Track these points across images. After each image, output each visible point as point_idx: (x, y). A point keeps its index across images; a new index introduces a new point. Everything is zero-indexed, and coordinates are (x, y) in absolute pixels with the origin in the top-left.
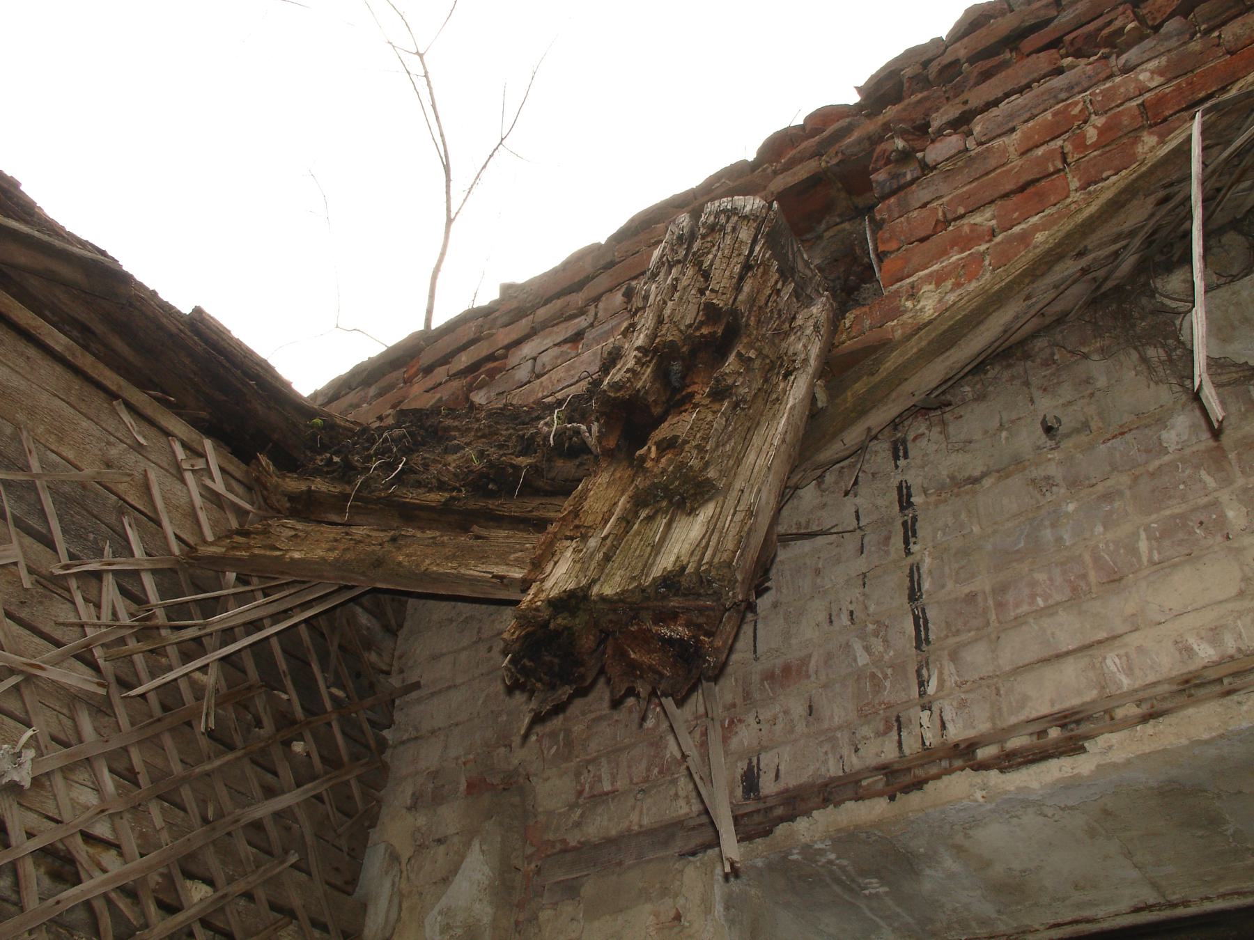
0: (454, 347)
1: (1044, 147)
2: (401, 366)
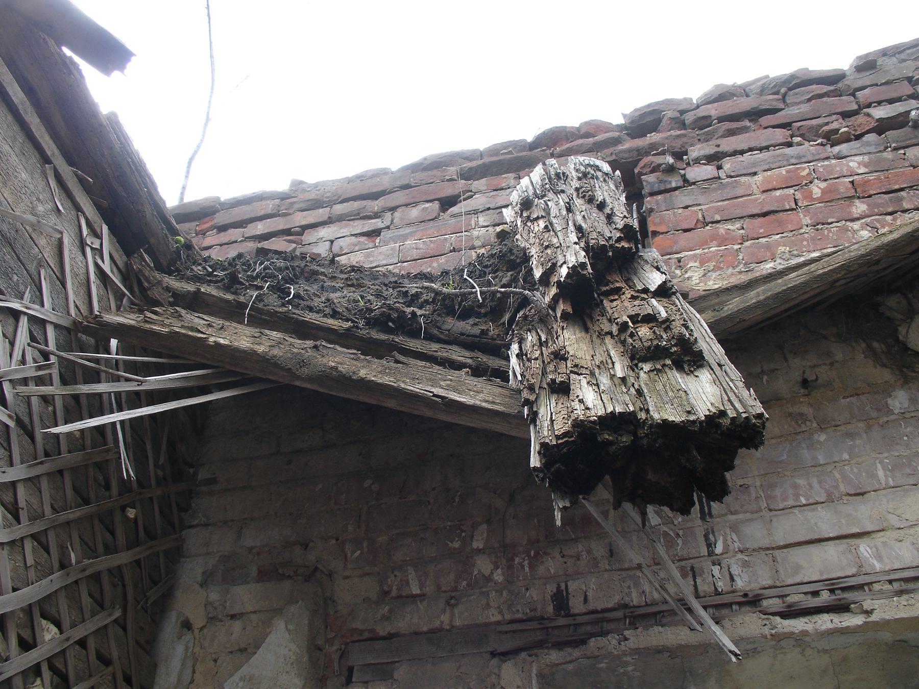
0: (252, 215)
1: (781, 191)
2: (194, 220)
